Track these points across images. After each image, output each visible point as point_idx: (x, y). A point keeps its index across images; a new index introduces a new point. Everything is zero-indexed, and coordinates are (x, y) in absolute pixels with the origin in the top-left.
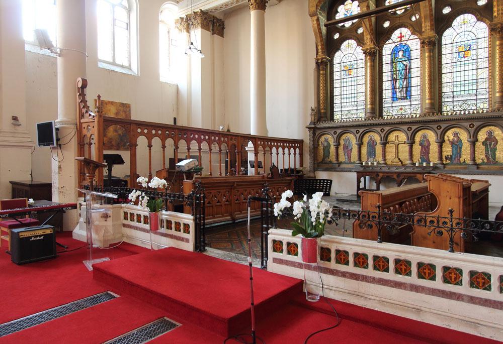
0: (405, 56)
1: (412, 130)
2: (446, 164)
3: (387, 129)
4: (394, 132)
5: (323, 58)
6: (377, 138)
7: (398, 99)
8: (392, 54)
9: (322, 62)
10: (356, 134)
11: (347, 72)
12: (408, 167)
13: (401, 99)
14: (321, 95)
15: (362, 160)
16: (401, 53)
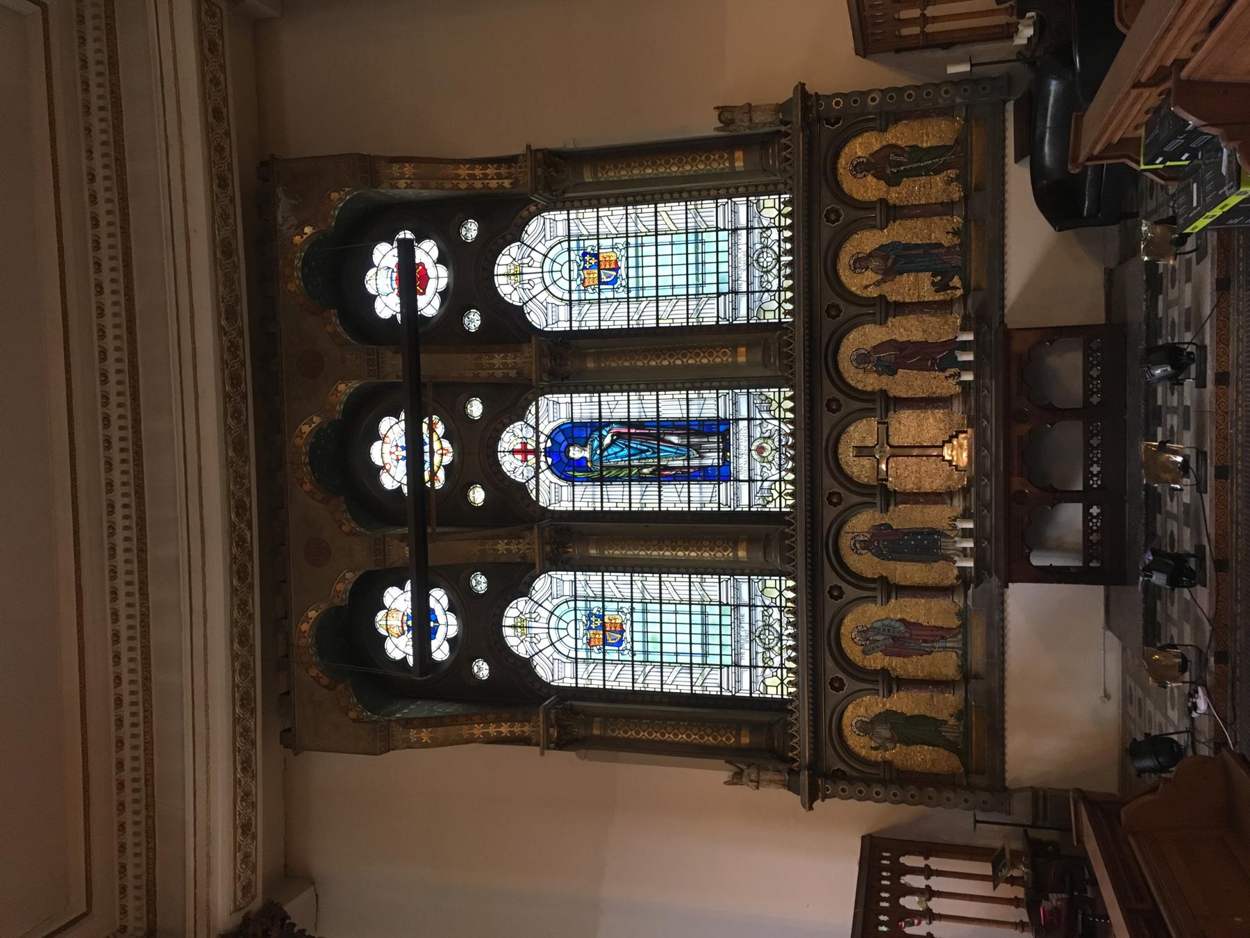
0: (587, 438)
2: (966, 287)
3: (829, 483)
5: (547, 716)
6: (863, 522)
7: (726, 463)
8: (572, 480)
10: (843, 411)
12: (978, 410)
13: (727, 449)
15: (951, 578)
16: (575, 453)
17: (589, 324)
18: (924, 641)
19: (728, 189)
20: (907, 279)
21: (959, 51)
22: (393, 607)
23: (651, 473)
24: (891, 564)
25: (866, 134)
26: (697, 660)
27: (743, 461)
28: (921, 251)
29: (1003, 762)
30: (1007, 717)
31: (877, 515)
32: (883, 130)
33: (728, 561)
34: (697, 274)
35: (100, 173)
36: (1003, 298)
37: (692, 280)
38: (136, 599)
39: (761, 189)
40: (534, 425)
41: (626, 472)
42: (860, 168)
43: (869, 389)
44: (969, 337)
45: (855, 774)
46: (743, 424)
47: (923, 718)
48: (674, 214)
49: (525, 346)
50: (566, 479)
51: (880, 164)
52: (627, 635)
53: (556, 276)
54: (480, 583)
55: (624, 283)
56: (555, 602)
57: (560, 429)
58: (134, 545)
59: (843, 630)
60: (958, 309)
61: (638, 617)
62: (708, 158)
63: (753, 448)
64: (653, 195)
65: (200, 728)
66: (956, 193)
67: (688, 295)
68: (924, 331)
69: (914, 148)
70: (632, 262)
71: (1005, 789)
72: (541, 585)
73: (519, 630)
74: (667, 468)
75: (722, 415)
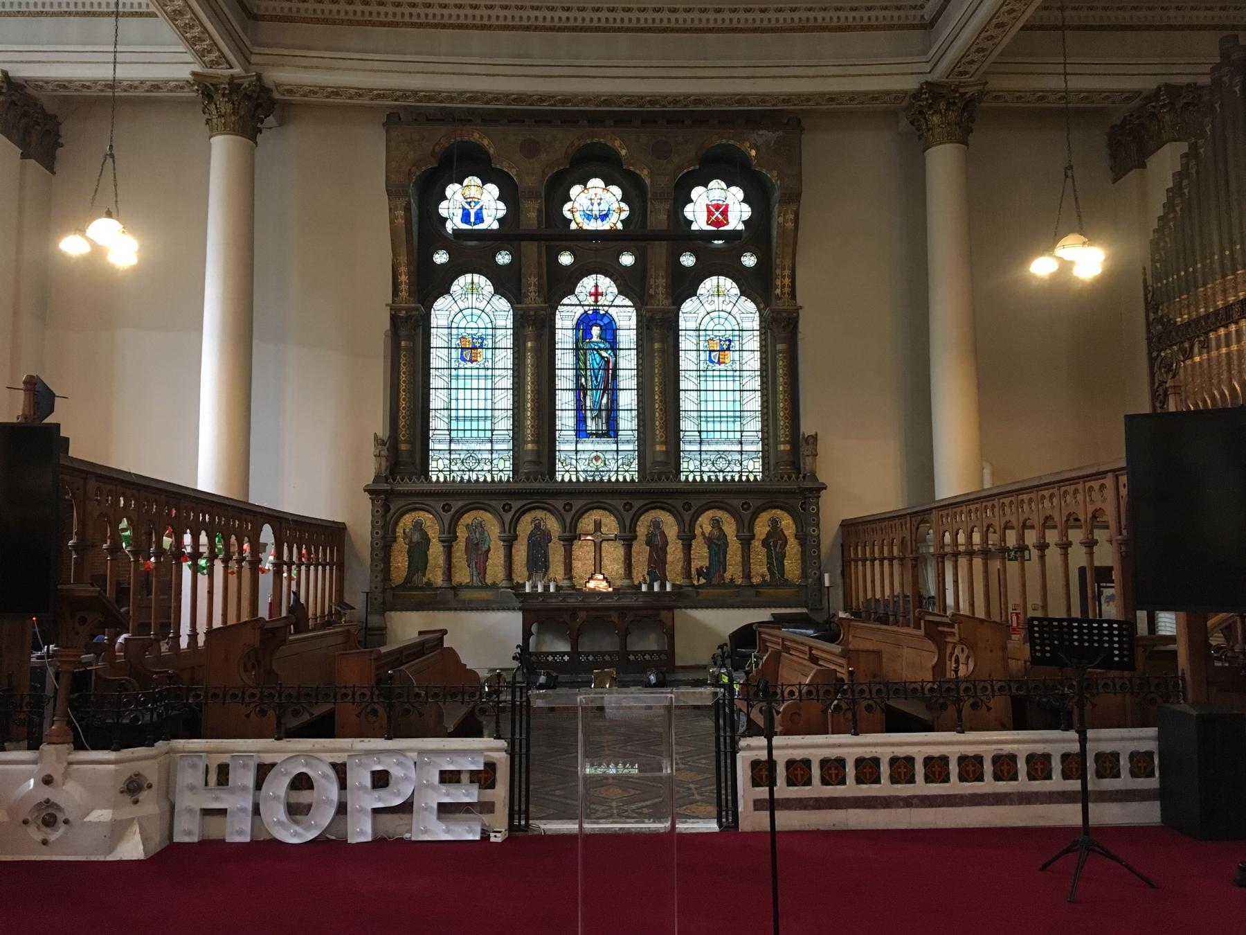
0: (605, 340)
1: (453, 510)
2: (699, 587)
3: (578, 504)
4: (591, 512)
5: (414, 309)
7: (589, 435)
8: (577, 328)
9: (408, 318)
10: (624, 513)
11: (467, 354)
12: (624, 594)
13: (597, 435)
14: (403, 404)
15: (518, 579)
16: (596, 331)
17: (683, 342)
18: (476, 563)
19: (767, 439)
20: (705, 552)
21: (839, 580)
22: (484, 191)
23: (582, 384)
24: (525, 542)
25: (794, 526)
26: (454, 413)
27: (590, 447)
28: (722, 560)
29: (402, 610)
30: (431, 612)
31: (557, 534)
32: (796, 537)
33: (524, 437)
34: (714, 417)
35: (796, 15)
36: (691, 608)
37: (710, 414)
38: (501, 22)
39: (766, 460)
40: (614, 303)
41: (583, 367)
42: (774, 523)
43: (638, 529)
44: (668, 588)
45: (388, 519)
46: (614, 447)
47: (427, 561)
48: (754, 402)
49: (670, 301)
50: (578, 324)
51: (776, 533)
52: (469, 365)
53: (716, 321)
54: (503, 259)
55: (709, 368)
56: (491, 314)
57: (612, 320)
58: (540, 23)
59: (481, 512)
60: (686, 582)
61: (482, 372)
62: (787, 427)
63: (598, 453)
64: (766, 389)
65: (411, 67)
66: (755, 580)
67: (700, 411)
68: (673, 562)
69: (784, 556)
70: (723, 373)
71: (385, 611)
72: (503, 304)
73: (470, 286)
74: (585, 395)
75: (620, 433)
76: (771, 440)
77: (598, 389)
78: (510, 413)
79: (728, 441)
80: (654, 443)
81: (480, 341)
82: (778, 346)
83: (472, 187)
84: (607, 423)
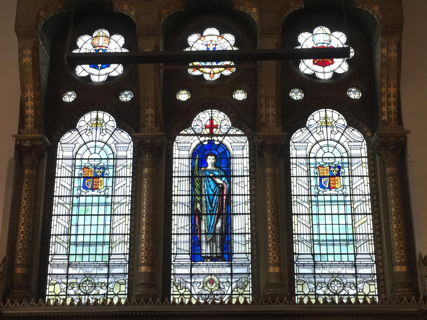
0: (220, 168)
5: (37, 139)
7: (203, 259)
8: (193, 157)
13: (212, 259)
16: (210, 160)
17: (294, 169)
19: (382, 261)
23: (197, 209)
26: (73, 239)
27: (204, 270)
34: (326, 240)
41: (198, 193)
49: (280, 128)
50: (194, 154)
52: (90, 193)
53: (325, 149)
55: (321, 193)
56: (113, 146)
57: (226, 149)
70: (334, 198)
74: (200, 220)
76: (386, 262)
77: (213, 214)
78: (127, 238)
79: (342, 264)
80: (268, 265)
81: (101, 170)
82: (387, 169)
83: (101, 38)
84: (222, 247)
